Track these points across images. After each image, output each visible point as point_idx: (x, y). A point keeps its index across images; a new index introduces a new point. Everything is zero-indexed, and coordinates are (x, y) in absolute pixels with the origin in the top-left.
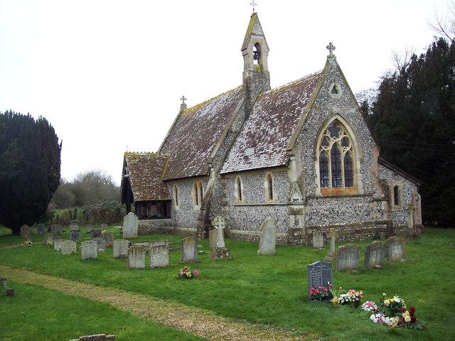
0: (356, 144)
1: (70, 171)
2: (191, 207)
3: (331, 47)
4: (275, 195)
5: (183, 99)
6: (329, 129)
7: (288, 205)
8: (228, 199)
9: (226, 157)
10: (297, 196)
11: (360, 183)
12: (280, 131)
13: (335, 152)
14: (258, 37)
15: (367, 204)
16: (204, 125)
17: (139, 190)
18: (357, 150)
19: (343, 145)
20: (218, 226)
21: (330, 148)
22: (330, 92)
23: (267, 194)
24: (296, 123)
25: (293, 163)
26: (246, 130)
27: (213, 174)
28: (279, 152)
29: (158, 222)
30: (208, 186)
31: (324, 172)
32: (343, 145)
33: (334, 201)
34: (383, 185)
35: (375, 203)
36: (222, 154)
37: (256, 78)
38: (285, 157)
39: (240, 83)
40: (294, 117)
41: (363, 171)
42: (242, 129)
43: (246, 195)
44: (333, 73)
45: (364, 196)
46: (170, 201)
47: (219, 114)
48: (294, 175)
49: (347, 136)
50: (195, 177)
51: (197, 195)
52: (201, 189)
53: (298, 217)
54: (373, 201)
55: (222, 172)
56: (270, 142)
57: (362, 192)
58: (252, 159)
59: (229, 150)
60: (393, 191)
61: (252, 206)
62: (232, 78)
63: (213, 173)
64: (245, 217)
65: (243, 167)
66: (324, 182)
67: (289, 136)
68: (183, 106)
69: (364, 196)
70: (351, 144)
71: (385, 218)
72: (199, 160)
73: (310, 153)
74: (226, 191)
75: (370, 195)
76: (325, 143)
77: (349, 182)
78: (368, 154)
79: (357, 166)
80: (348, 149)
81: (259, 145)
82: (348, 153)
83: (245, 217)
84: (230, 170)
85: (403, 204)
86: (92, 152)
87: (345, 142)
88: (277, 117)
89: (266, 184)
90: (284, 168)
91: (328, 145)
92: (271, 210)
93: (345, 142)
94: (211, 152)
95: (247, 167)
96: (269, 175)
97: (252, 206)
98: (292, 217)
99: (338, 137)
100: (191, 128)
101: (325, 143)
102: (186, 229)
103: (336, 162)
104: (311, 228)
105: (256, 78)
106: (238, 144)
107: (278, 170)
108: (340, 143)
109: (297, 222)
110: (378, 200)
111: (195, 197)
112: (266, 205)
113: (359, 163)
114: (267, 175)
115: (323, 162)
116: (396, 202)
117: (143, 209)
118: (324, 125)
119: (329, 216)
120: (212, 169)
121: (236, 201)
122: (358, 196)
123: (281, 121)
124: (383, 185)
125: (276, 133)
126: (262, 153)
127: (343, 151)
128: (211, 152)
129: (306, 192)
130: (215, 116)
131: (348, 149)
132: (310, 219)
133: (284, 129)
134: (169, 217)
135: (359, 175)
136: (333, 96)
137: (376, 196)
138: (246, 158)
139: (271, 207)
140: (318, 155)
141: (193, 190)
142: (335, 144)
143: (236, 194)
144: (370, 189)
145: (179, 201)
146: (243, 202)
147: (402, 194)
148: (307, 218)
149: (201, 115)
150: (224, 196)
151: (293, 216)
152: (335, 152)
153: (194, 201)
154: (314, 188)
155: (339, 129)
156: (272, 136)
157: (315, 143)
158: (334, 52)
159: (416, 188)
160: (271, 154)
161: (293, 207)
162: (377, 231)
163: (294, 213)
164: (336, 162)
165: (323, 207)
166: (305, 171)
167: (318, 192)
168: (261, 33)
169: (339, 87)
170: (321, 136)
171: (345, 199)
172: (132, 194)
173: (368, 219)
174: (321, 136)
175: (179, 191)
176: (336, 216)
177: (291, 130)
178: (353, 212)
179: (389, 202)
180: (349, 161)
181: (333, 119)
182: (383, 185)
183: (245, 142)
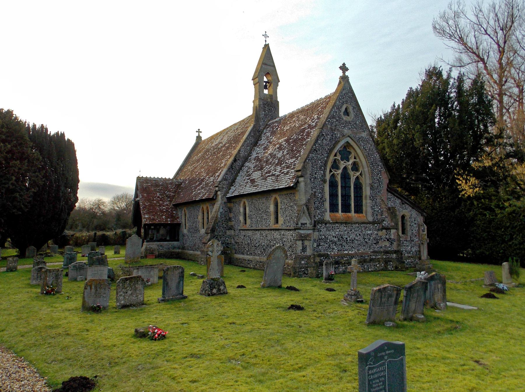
0: (366, 169)
1: (85, 198)
2: (197, 231)
3: (344, 68)
4: (281, 219)
6: (340, 151)
7: (295, 229)
8: (233, 223)
9: (234, 181)
10: (305, 220)
11: (369, 210)
12: (288, 154)
13: (345, 176)
14: (269, 67)
15: (376, 232)
16: (214, 153)
17: (148, 213)
18: (367, 175)
19: (353, 169)
20: (212, 252)
21: (340, 171)
22: (342, 113)
23: (272, 218)
24: (306, 144)
25: (302, 185)
26: (254, 155)
27: (220, 197)
28: (287, 173)
29: (167, 245)
30: (214, 210)
31: (333, 196)
32: (353, 169)
33: (343, 228)
34: (392, 213)
35: (384, 231)
37: (266, 104)
38: (293, 178)
39: (249, 112)
40: (303, 139)
41: (372, 198)
42: (250, 154)
43: (251, 219)
44: (345, 94)
45: (373, 223)
46: (179, 225)
47: (229, 142)
48: (302, 197)
49: (358, 160)
50: (202, 201)
51: (203, 219)
52: (208, 213)
53: (306, 243)
54: (382, 229)
55: (229, 195)
56: (277, 165)
57: (370, 219)
58: (259, 182)
59: (237, 175)
60: (400, 220)
61: (257, 230)
62: (241, 107)
63: (220, 197)
64: (249, 241)
65: (249, 189)
66: (333, 208)
67: (298, 157)
68: (199, 138)
69: (373, 223)
70: (361, 170)
71: (394, 247)
72: (207, 185)
73: (319, 176)
74: (231, 215)
75: (379, 222)
76: (335, 166)
77: (359, 209)
78: (378, 180)
79: (367, 191)
80: (358, 174)
81: (267, 168)
82: (357, 178)
83: (249, 241)
84: (236, 193)
85: (409, 233)
86: (105, 176)
87: (355, 167)
88: (285, 140)
89: (272, 208)
90: (291, 190)
91: (338, 168)
92: (276, 235)
93: (355, 167)
94: (218, 176)
95: (253, 190)
96: (276, 198)
97: (257, 230)
99: (348, 161)
100: (203, 156)
101: (335, 166)
102: (346, 252)
103: (346, 187)
104: (320, 256)
105: (266, 104)
106: (245, 169)
107: (285, 192)
108: (350, 167)
109: (304, 249)
110: (387, 229)
111: (201, 221)
112: (271, 230)
113: (368, 188)
114: (273, 199)
115: (333, 185)
116: (403, 233)
117: (148, 232)
119: (338, 243)
120: (219, 193)
121: (241, 225)
122: (368, 223)
123: (289, 144)
124: (392, 212)
125: (284, 156)
126: (269, 176)
127: (353, 176)
128: (218, 176)
129: (315, 216)
130: (225, 144)
131: (358, 174)
132: (318, 246)
133: (292, 150)
134: (178, 240)
135: (369, 201)
136: (345, 118)
138: (253, 181)
139: (277, 232)
140: (328, 177)
141: (200, 214)
142: (345, 168)
143: (241, 218)
144: (379, 217)
145: (187, 225)
146: (248, 226)
147: (409, 224)
148: (315, 245)
149: (213, 145)
150: (230, 219)
151: (301, 242)
152: (345, 176)
153: (200, 225)
154: (324, 212)
155: (350, 153)
156: (280, 158)
158: (347, 73)
159: (422, 218)
160: (278, 176)
161: (302, 232)
162: (387, 262)
163: (303, 238)
164: (346, 187)
165: (332, 234)
166: (314, 195)
167: (328, 216)
168: (272, 64)
169: (351, 109)
170: (332, 158)
171: (354, 226)
172: (141, 216)
173: (376, 248)
174: (332, 158)
175: (187, 215)
176: (344, 244)
177: (299, 152)
178: (362, 240)
179: (397, 229)
180: (358, 187)
181: (342, 143)
182: (392, 212)
183: (252, 166)
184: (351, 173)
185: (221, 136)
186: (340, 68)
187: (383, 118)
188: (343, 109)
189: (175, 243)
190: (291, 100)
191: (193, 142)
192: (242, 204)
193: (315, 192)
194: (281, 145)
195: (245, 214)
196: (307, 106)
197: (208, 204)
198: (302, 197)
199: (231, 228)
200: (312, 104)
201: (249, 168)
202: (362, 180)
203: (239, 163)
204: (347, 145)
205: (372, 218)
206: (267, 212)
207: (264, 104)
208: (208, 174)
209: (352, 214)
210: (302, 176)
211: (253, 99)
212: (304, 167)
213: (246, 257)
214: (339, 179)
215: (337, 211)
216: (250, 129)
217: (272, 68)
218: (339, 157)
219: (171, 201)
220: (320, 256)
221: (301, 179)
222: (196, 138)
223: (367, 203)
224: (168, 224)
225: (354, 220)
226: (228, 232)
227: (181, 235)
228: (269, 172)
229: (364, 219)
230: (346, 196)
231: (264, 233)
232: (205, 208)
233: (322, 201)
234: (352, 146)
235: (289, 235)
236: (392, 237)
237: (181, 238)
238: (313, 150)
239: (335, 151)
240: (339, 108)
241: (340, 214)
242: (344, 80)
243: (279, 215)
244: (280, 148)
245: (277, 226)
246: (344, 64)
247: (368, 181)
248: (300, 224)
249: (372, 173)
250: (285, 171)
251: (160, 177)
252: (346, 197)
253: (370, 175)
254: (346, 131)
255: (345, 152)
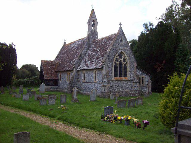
0: (128, 61)
2: (66, 82)
3: (121, 24)
4: (97, 79)
5: (65, 40)
6: (119, 55)
11: (129, 76)
13: (120, 64)
14: (94, 18)
17: (46, 75)
21: (118, 62)
22: (119, 41)
23: (94, 78)
24: (106, 52)
26: (88, 54)
31: (116, 71)
36: (78, 63)
39: (87, 35)
42: (86, 53)
43: (86, 78)
45: (130, 81)
46: (58, 79)
48: (104, 72)
50: (67, 71)
51: (68, 78)
53: (105, 88)
54: (134, 83)
57: (130, 79)
58: (89, 65)
60: (141, 79)
62: (83, 33)
65: (85, 68)
66: (116, 75)
68: (65, 43)
71: (138, 89)
72: (69, 64)
73: (111, 64)
75: (133, 80)
77: (125, 76)
79: (128, 69)
80: (125, 63)
84: (81, 69)
87: (124, 60)
88: (99, 49)
89: (94, 75)
90: (101, 69)
92: (96, 85)
93: (124, 60)
94: (74, 61)
95: (87, 68)
96: (95, 72)
98: (103, 88)
99: (122, 58)
101: (117, 60)
103: (121, 68)
105: (93, 34)
109: (105, 90)
110: (135, 82)
111: (67, 78)
113: (129, 68)
114: (94, 72)
115: (116, 67)
118: (116, 53)
123: (101, 51)
127: (124, 63)
128: (74, 61)
134: (58, 86)
135: (129, 73)
136: (121, 43)
137: (135, 81)
138: (87, 65)
143: (83, 78)
146: (85, 81)
150: (78, 78)
152: (120, 64)
153: (67, 80)
154: (112, 77)
155: (122, 55)
157: (113, 60)
158: (122, 26)
163: (104, 86)
164: (121, 68)
165: (115, 85)
167: (113, 78)
169: (123, 40)
170: (115, 58)
173: (131, 89)
174: (115, 58)
175: (61, 76)
177: (104, 55)
180: (125, 68)
181: (120, 52)
183: (87, 58)
184: (123, 63)
185: (74, 44)
186: (119, 24)
187: (159, 23)
188: (120, 40)
189: (57, 87)
190: (102, 34)
191: (62, 45)
192: (83, 73)
193: (109, 70)
194: (98, 51)
195: (84, 77)
196: (108, 36)
197: (70, 72)
198: (104, 72)
199: (79, 82)
200: (110, 36)
201: (86, 59)
202: (127, 65)
203: (82, 57)
204: (122, 52)
205: (130, 79)
206: (92, 76)
207: (92, 33)
208: (69, 60)
209: (123, 77)
210: (104, 65)
211: (88, 31)
212: (105, 61)
213: (84, 92)
214: (118, 65)
215: (117, 76)
216: (86, 43)
217: (95, 19)
218: (118, 57)
219: (54, 70)
220: (110, 92)
221: (104, 66)
222: (63, 43)
223: (128, 74)
224: (54, 79)
225: (123, 79)
226: (78, 83)
227: (59, 83)
228: (93, 62)
229: (127, 79)
230: (121, 71)
231: (91, 84)
232: (69, 73)
233: (112, 73)
234: (123, 53)
235: (100, 85)
236: (137, 85)
237: (59, 85)
238: (109, 55)
239: (117, 55)
240: (118, 39)
241: (118, 78)
242: (121, 29)
243: (97, 78)
244: (97, 53)
245: (96, 82)
246: (121, 23)
247: (129, 66)
248: (103, 81)
249: (130, 62)
250: (99, 62)
251: (50, 60)
252: (121, 71)
253: (131, 63)
254: (121, 48)
255: (121, 55)
